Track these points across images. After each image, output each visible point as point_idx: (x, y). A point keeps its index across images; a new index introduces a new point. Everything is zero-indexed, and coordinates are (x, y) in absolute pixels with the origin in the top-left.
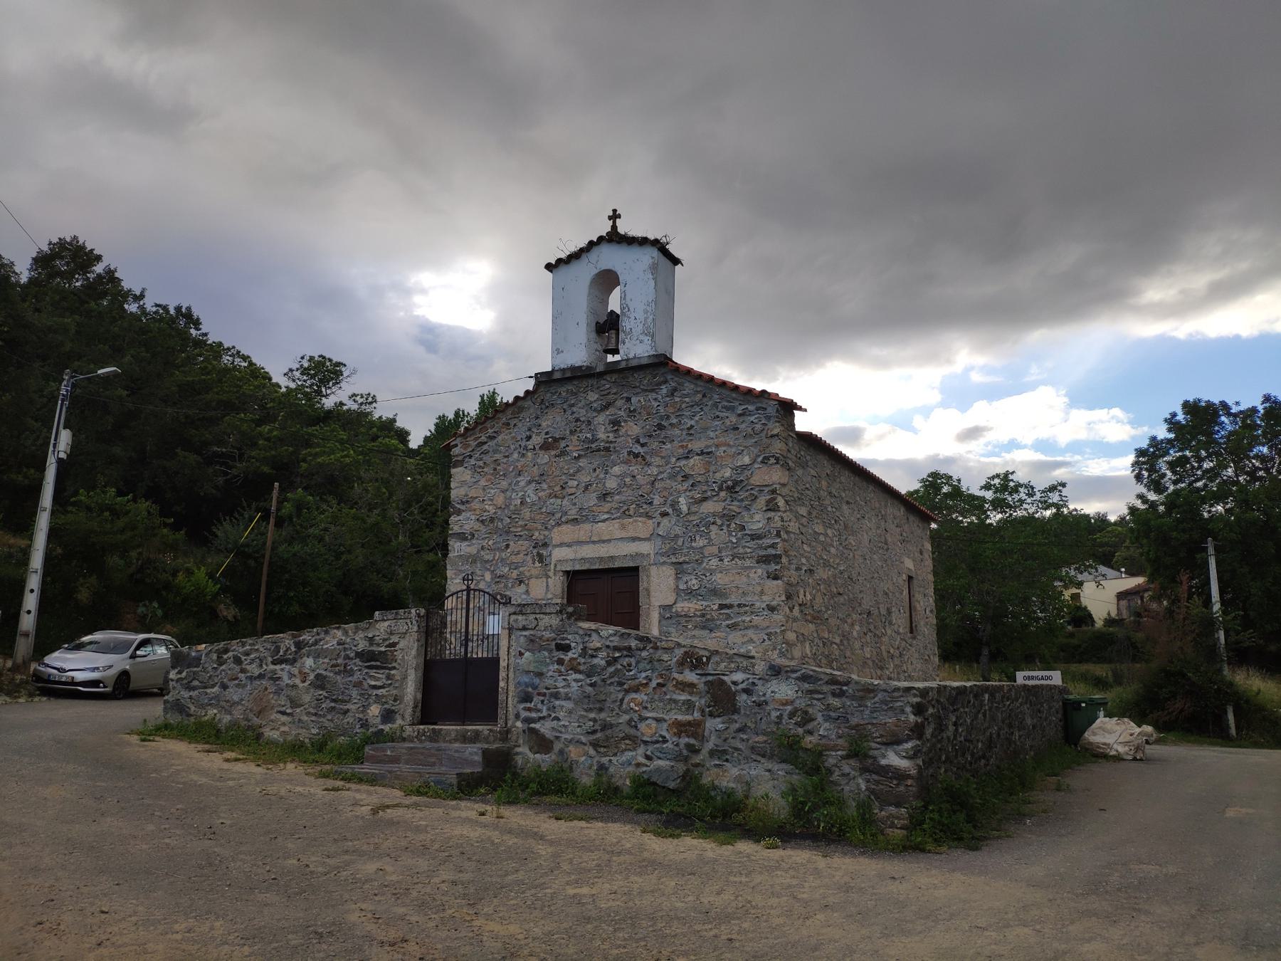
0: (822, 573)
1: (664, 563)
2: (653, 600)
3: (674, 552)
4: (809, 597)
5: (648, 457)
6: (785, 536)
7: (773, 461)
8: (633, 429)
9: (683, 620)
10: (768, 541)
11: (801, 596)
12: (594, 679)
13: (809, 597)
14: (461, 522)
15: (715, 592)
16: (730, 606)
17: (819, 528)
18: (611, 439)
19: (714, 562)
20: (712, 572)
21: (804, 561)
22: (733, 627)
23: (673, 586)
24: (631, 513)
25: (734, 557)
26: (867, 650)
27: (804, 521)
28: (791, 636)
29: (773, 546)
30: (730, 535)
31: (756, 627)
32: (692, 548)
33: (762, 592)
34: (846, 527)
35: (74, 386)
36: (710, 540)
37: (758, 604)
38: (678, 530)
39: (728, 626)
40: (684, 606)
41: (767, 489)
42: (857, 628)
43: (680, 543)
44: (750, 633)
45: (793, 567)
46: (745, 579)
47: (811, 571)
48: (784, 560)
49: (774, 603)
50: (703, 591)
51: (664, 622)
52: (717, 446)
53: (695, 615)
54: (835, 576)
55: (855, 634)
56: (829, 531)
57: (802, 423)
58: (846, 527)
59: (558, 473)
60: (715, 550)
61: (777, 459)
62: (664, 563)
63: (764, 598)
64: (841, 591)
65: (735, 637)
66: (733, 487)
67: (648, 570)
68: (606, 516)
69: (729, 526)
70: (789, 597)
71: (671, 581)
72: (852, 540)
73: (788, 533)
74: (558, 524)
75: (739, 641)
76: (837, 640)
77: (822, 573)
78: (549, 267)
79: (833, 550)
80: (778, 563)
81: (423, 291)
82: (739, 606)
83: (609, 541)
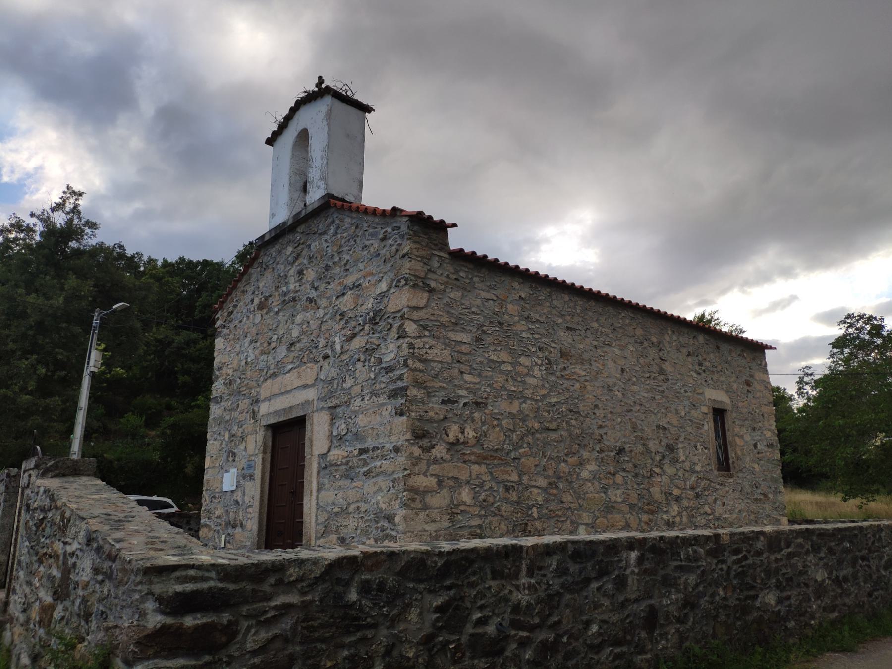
1: (322, 408)
2: (314, 448)
5: (318, 300)
7: (403, 282)
8: (310, 275)
9: (333, 469)
10: (398, 373)
12: (359, 531)
14: (218, 387)
15: (358, 436)
18: (298, 288)
19: (358, 402)
20: (356, 413)
21: (462, 392)
22: (367, 474)
23: (327, 433)
29: (400, 378)
30: (370, 371)
31: (384, 473)
32: (343, 389)
35: (101, 319)
38: (334, 372)
41: (399, 315)
43: (335, 386)
44: (380, 479)
46: (378, 418)
48: (413, 392)
52: (364, 277)
57: (456, 240)
59: (265, 330)
60: (357, 389)
61: (406, 280)
65: (369, 486)
66: (374, 318)
68: (290, 367)
78: (270, 142)
81: (547, 240)
83: (291, 390)
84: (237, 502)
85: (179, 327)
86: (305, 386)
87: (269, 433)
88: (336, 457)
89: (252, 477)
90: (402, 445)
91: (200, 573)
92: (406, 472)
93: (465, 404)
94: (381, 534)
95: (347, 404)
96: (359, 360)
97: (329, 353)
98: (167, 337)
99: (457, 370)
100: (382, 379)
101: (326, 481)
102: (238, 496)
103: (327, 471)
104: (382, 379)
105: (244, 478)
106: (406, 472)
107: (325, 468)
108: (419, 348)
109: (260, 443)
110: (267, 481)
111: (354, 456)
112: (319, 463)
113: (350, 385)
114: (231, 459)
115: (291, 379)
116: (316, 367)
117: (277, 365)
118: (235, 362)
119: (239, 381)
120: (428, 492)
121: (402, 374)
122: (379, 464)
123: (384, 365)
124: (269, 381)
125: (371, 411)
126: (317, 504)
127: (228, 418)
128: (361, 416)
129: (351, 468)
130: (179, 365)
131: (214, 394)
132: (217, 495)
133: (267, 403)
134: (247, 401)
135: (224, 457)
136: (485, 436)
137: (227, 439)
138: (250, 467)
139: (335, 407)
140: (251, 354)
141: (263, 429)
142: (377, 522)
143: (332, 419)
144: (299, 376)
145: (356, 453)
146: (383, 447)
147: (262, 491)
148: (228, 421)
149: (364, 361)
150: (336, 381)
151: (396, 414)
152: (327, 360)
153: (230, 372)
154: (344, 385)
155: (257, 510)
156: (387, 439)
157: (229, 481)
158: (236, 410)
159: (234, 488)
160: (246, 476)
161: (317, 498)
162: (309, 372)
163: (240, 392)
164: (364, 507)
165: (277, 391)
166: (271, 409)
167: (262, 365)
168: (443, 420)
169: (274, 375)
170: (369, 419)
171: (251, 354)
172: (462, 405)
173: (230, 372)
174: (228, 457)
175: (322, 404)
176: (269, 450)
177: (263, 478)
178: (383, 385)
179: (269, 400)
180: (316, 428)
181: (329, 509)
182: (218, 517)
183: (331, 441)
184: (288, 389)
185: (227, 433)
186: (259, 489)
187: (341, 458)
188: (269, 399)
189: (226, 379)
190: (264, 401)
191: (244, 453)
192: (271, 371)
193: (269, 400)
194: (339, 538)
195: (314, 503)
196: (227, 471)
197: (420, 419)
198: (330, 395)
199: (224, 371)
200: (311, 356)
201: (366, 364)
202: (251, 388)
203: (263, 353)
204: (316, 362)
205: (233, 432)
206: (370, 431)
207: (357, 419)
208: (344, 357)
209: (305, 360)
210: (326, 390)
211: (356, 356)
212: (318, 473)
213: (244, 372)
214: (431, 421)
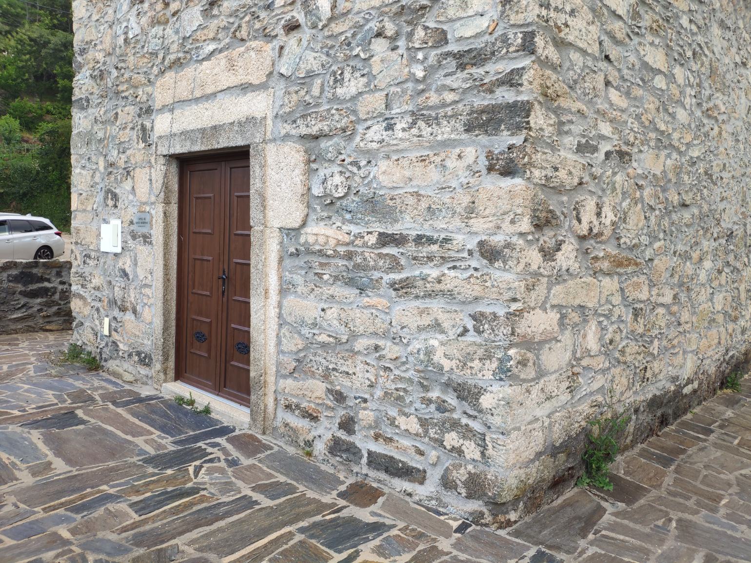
0: (649, 162)
1: (287, 137)
2: (270, 214)
3: (305, 110)
4: (609, 216)
6: (551, 52)
9: (316, 261)
10: (497, 68)
11: (588, 215)
13: (609, 216)
14: (83, 84)
15: (374, 205)
16: (398, 240)
17: (656, 58)
19: (377, 131)
20: (371, 157)
21: (605, 129)
22: (403, 287)
23: (300, 189)
24: (244, 33)
25: (416, 116)
26: (719, 298)
27: (617, 26)
28: (540, 322)
29: (511, 80)
30: (413, 60)
31: (449, 295)
32: (335, 99)
33: (471, 210)
34: (713, 72)
36: (370, 76)
37: (459, 238)
38: (313, 61)
39: (392, 285)
40: (323, 233)
42: (708, 264)
43: (316, 91)
44: (436, 306)
45: (570, 141)
46: (434, 175)
47: (623, 156)
48: (539, 119)
49: (498, 240)
50: (352, 202)
51: (288, 262)
53: (336, 255)
54: (678, 170)
55: (703, 276)
56: (678, 71)
58: (713, 72)
60: (376, 101)
62: (287, 137)
63: (478, 224)
64: (688, 198)
65: (406, 312)
67: (262, 153)
68: (211, 47)
69: (410, 35)
70: (543, 221)
71: (298, 176)
72: (719, 100)
73: (561, 44)
74: (162, 73)
75: (414, 322)
76: (668, 299)
77: (649, 162)
79: (682, 115)
80: (517, 128)
82: (419, 240)
83: (214, 95)
84: (125, 274)
85: (55, 27)
86: (245, 88)
87: (174, 169)
88: (322, 240)
89: (146, 239)
90: (508, 245)
91: (18, 551)
92: (514, 306)
93: (608, 154)
94: (438, 415)
95: (348, 133)
96: (379, 35)
97: (301, 17)
98: (41, 36)
99: (601, 78)
100: (448, 81)
101: (298, 279)
102: (126, 263)
103: (300, 262)
104: (448, 81)
105: (134, 237)
106: (514, 306)
107: (297, 254)
108: (556, 9)
109: (158, 185)
110: (175, 249)
111: (365, 245)
112: (281, 243)
113: (353, 91)
114: (110, 203)
115: (214, 73)
116: (269, 49)
117: (182, 45)
118: (108, 40)
119: (115, 73)
120: (545, 342)
121: (520, 72)
122: (434, 273)
123: (453, 47)
124: (170, 76)
125: (413, 155)
126: (280, 316)
127: (100, 135)
128: (383, 165)
129: (357, 266)
130: (58, 68)
131: (77, 94)
132: (93, 254)
133: (167, 116)
134: (132, 110)
135: (100, 197)
136: (625, 222)
137: (101, 168)
138: (142, 222)
139: (316, 138)
140: (133, 22)
141: (162, 161)
142: (426, 389)
143: (309, 162)
144: (231, 66)
145: (372, 239)
146: (446, 240)
147: (166, 266)
148: (100, 141)
149: (394, 38)
150: (318, 81)
151: (490, 169)
152: (295, 35)
153: (100, 56)
154: (340, 91)
155: (160, 295)
156: (457, 222)
157: (110, 237)
158: (113, 124)
159: (118, 250)
160: (137, 233)
161: (280, 306)
162: (255, 59)
163: (117, 93)
164: (391, 350)
165: (185, 95)
166: (184, 124)
167: (153, 45)
168: (575, 189)
169: (178, 64)
170: (408, 173)
171: (133, 22)
172: (602, 156)
173: (100, 56)
174: (106, 198)
175: (287, 128)
176: (175, 198)
177: (166, 245)
178: (450, 97)
179: (172, 111)
180: (272, 174)
181: (305, 331)
182: (97, 289)
183: (308, 206)
184: (209, 91)
185: (102, 159)
186: (161, 262)
187: (332, 242)
188: (170, 108)
189: (93, 69)
190: (161, 110)
191: (131, 197)
192: (173, 57)
193: (172, 111)
194: (329, 391)
195: (273, 312)
196: (106, 221)
197: (547, 186)
198: (305, 110)
199: (90, 55)
200: (258, 25)
201: (401, 43)
202: (137, 87)
203: (155, 22)
204: (269, 37)
205: (111, 159)
206: (411, 201)
207: (374, 171)
208: (337, 28)
209: (244, 33)
210: (295, 97)
211: (374, 25)
212: (281, 260)
213: (122, 58)
214: (559, 190)
